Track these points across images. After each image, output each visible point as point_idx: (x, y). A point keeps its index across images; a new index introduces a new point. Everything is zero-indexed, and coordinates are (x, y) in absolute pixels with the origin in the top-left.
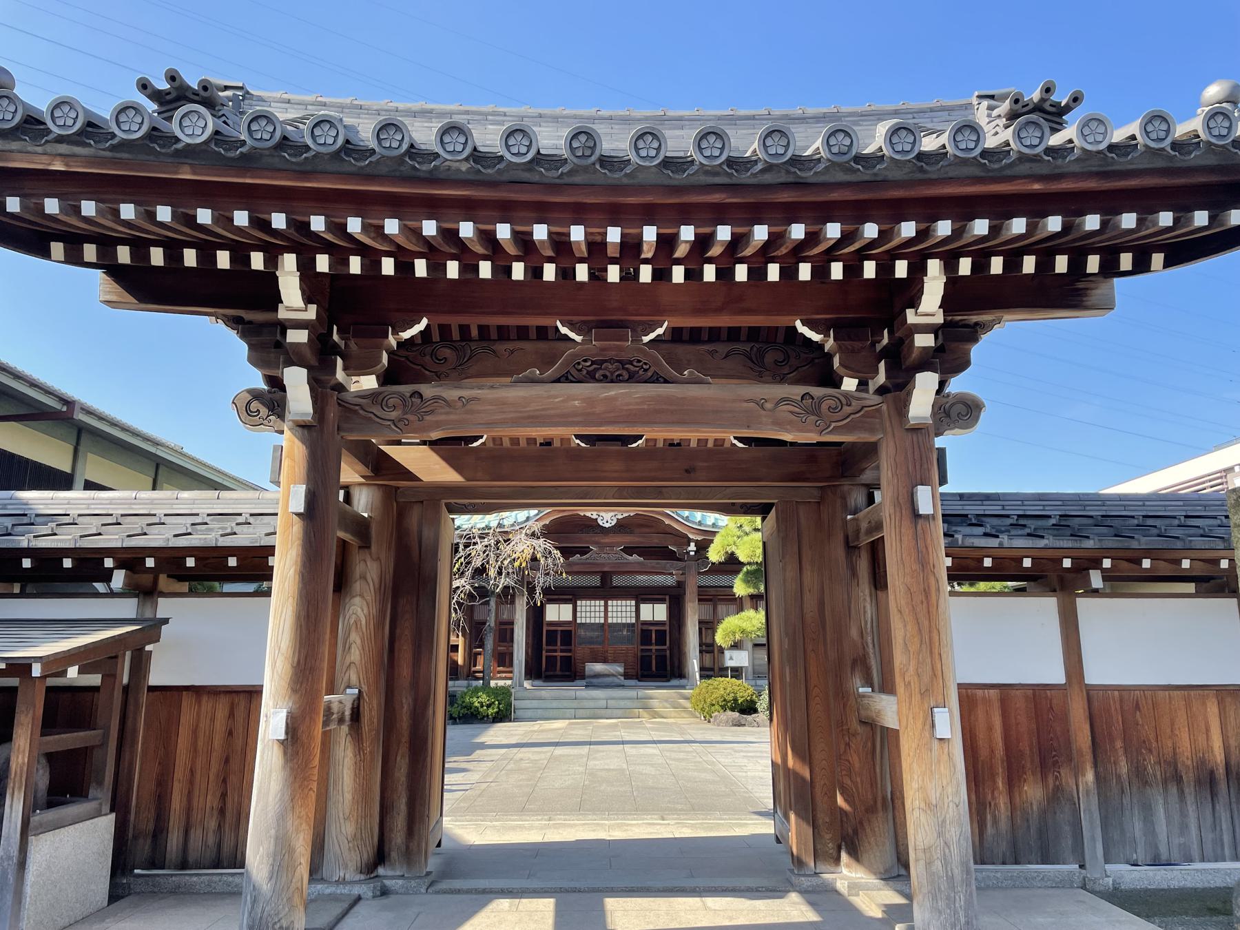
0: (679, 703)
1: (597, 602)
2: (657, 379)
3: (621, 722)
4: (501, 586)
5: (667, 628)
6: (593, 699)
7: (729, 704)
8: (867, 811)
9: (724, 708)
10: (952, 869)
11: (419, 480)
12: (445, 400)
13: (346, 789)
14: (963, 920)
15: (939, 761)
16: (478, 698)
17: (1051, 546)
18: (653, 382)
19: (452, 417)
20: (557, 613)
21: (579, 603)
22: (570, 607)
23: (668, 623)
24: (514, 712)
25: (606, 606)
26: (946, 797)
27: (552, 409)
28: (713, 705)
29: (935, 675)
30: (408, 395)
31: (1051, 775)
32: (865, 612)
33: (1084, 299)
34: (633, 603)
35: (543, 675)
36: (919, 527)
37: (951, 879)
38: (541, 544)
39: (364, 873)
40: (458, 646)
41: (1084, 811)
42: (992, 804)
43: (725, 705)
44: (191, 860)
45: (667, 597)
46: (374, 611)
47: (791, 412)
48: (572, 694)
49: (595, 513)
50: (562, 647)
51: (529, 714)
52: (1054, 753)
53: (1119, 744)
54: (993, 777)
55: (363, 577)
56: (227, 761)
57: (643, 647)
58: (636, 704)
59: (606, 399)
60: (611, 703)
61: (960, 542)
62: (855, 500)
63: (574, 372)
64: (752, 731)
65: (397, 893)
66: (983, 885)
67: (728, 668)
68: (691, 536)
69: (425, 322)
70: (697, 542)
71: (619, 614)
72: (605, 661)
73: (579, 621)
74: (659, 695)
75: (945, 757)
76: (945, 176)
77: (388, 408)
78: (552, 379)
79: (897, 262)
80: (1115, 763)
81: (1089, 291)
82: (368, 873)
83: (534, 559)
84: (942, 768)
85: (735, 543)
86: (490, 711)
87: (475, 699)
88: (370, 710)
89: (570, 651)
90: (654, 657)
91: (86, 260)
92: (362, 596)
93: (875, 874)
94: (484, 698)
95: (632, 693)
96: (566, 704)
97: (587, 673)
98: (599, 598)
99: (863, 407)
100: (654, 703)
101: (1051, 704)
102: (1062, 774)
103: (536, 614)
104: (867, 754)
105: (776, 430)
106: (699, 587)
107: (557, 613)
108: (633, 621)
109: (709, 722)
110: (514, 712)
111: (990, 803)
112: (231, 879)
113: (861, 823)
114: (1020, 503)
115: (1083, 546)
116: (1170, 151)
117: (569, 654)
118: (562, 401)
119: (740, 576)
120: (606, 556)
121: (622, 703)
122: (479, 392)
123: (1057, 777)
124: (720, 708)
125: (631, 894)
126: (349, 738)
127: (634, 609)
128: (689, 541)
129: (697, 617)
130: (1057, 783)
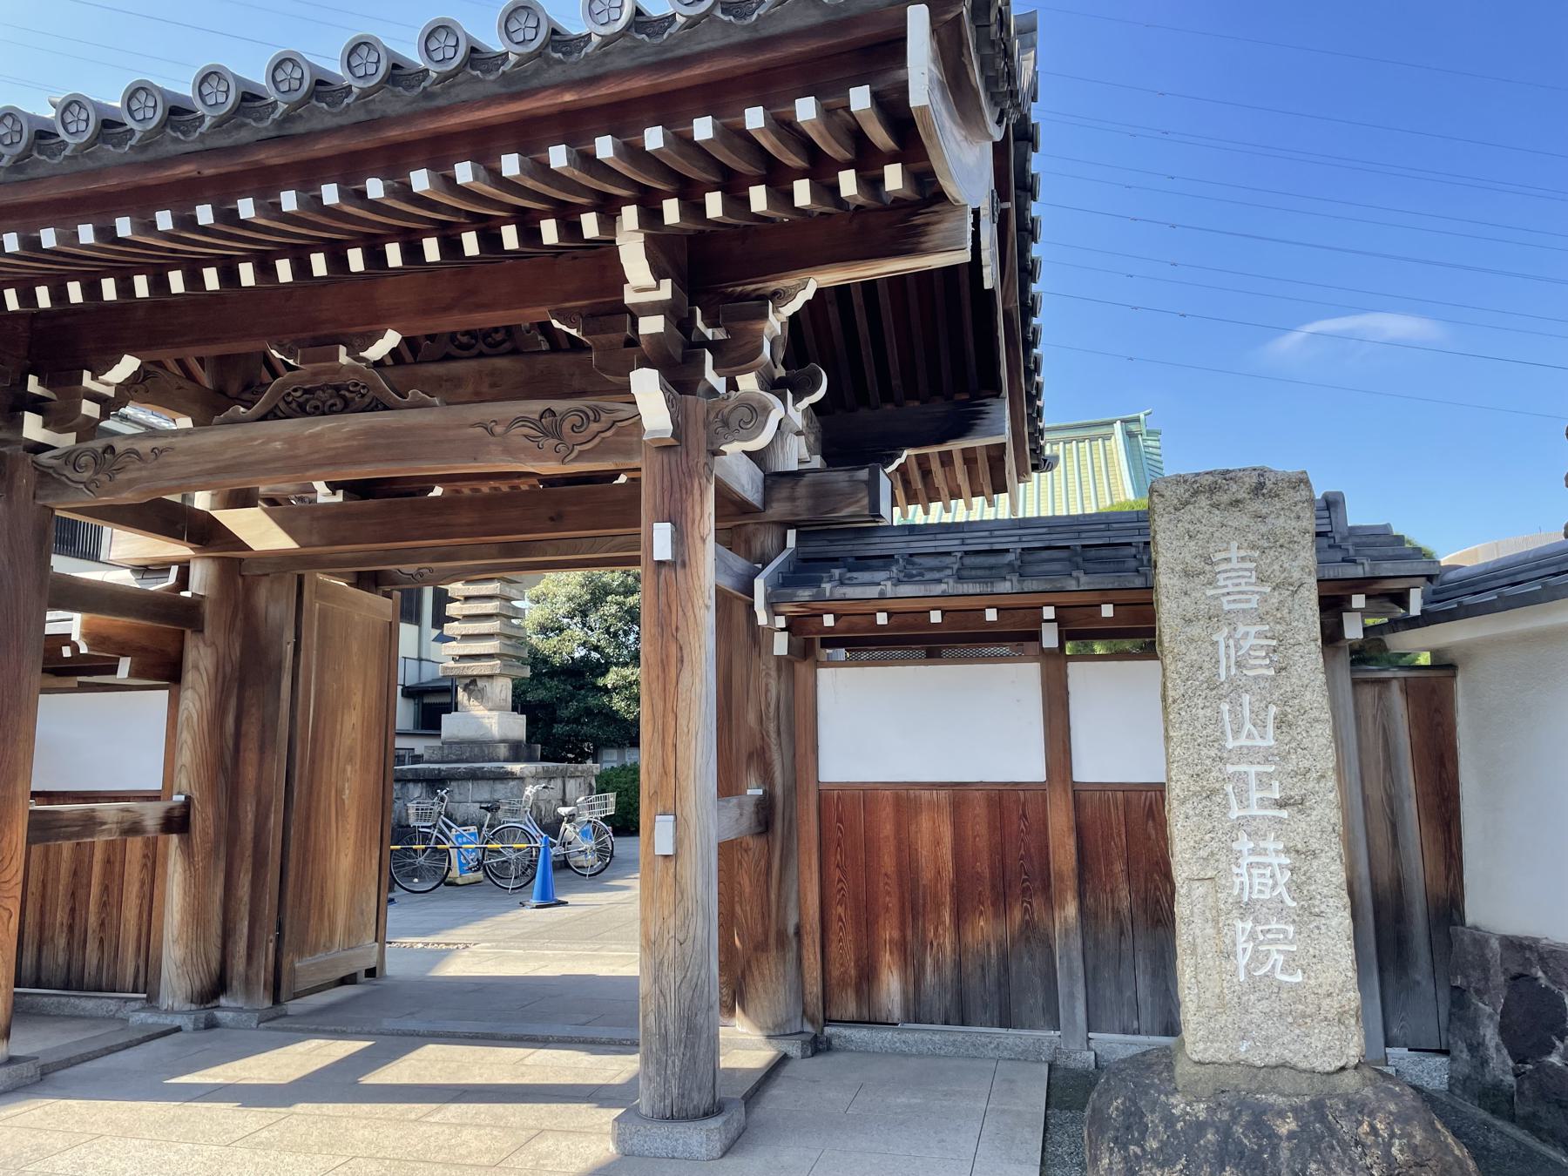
2: (378, 405)
8: (756, 949)
10: (665, 1026)
11: (248, 548)
12: (137, 453)
13: (175, 909)
14: (675, 1091)
15: (661, 885)
17: (951, 592)
18: (372, 410)
19: (144, 473)
26: (666, 933)
27: (250, 454)
29: (666, 774)
30: (100, 450)
31: (1018, 906)
32: (767, 691)
33: (923, 239)
36: (662, 578)
37: (664, 1038)
39: (195, 1003)
41: (1060, 958)
42: (935, 944)
44: (44, 979)
46: (208, 705)
47: (525, 436)
52: (1024, 877)
53: (1119, 867)
54: (938, 906)
55: (196, 667)
56: (75, 873)
59: (311, 436)
61: (828, 594)
62: (763, 542)
63: (282, 405)
65: (228, 1027)
66: (914, 1050)
69: (273, 351)
75: (670, 879)
76: (457, 100)
77: (81, 468)
78: (255, 418)
79: (543, 223)
80: (1112, 891)
81: (931, 228)
82: (202, 1003)
84: (665, 894)
88: (204, 821)
92: (193, 688)
93: (761, 1029)
99: (615, 422)
101: (1024, 811)
102: (1034, 905)
104: (759, 875)
105: (509, 461)
111: (932, 944)
112: (77, 1001)
113: (749, 962)
114: (986, 534)
115: (995, 591)
116: (722, 16)
118: (263, 443)
122: (174, 440)
123: (1026, 909)
125: (358, 1036)
126: (179, 850)
130: (1027, 917)
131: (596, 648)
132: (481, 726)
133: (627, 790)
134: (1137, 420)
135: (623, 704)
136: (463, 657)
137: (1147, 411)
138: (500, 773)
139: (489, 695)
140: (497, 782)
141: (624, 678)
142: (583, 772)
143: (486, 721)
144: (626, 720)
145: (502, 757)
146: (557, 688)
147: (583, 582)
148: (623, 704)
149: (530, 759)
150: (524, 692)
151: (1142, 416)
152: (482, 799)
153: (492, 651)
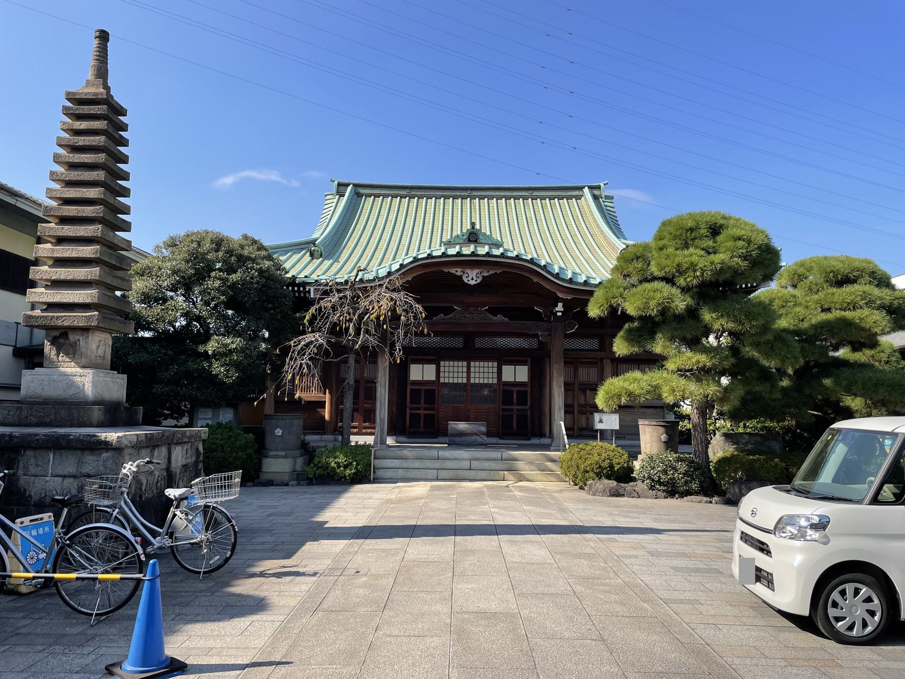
0: (547, 466)
1: (460, 363)
3: (487, 486)
4: (360, 343)
5: (529, 389)
6: (456, 459)
7: (604, 472)
9: (599, 475)
16: (335, 458)
20: (419, 372)
21: (442, 363)
22: (434, 367)
23: (529, 384)
24: (374, 472)
25: (469, 367)
28: (587, 472)
34: (495, 364)
35: (407, 432)
38: (401, 296)
40: (325, 401)
43: (600, 472)
45: (529, 360)
48: (434, 453)
49: (459, 270)
50: (426, 406)
51: (389, 474)
57: (504, 407)
58: (500, 465)
60: (475, 464)
64: (636, 506)
67: (597, 431)
68: (560, 295)
70: (565, 302)
71: (482, 375)
72: (466, 419)
73: (442, 380)
74: (525, 457)
83: (395, 318)
85: (621, 296)
86: (348, 472)
87: (331, 460)
89: (433, 409)
90: (515, 416)
91: (434, 379)
94: (341, 459)
95: (495, 454)
96: (428, 464)
97: (449, 432)
98: (462, 360)
100: (520, 465)
103: (399, 373)
106: (565, 350)
107: (419, 372)
108: (495, 381)
109: (581, 488)
110: (374, 472)
117: (432, 412)
119: (621, 333)
120: (470, 316)
121: (486, 465)
124: (594, 475)
127: (495, 370)
128: (558, 300)
129: (562, 378)
131: (198, 318)
132: (72, 384)
133: (222, 446)
134: (599, 187)
135: (222, 369)
136: (52, 306)
137: (606, 182)
138: (90, 442)
139: (83, 350)
140: (87, 452)
141: (226, 346)
142: (191, 437)
143: (78, 379)
144: (225, 383)
145: (95, 421)
146: (159, 352)
147: (188, 258)
148: (222, 369)
149: (130, 423)
150: (126, 355)
151: (602, 185)
152: (66, 473)
153: (88, 301)
